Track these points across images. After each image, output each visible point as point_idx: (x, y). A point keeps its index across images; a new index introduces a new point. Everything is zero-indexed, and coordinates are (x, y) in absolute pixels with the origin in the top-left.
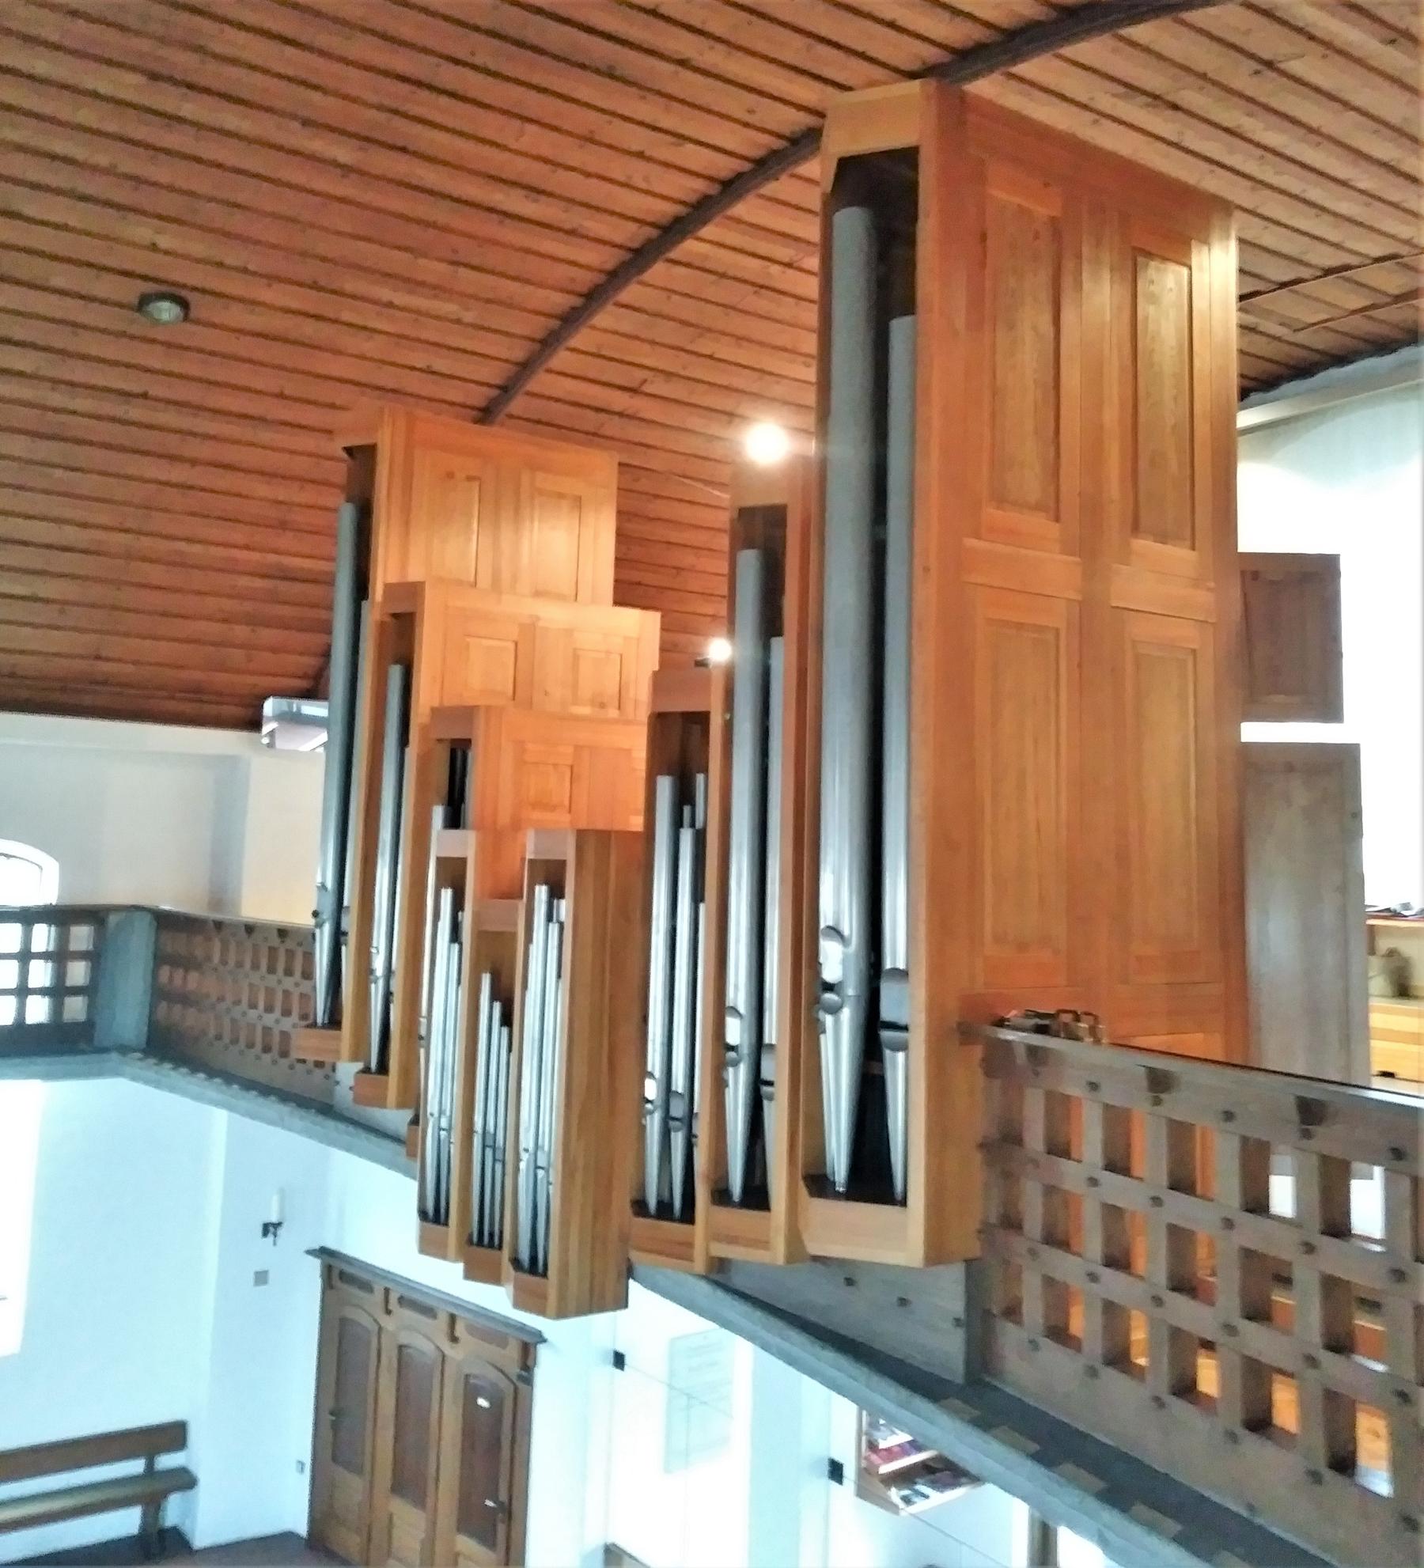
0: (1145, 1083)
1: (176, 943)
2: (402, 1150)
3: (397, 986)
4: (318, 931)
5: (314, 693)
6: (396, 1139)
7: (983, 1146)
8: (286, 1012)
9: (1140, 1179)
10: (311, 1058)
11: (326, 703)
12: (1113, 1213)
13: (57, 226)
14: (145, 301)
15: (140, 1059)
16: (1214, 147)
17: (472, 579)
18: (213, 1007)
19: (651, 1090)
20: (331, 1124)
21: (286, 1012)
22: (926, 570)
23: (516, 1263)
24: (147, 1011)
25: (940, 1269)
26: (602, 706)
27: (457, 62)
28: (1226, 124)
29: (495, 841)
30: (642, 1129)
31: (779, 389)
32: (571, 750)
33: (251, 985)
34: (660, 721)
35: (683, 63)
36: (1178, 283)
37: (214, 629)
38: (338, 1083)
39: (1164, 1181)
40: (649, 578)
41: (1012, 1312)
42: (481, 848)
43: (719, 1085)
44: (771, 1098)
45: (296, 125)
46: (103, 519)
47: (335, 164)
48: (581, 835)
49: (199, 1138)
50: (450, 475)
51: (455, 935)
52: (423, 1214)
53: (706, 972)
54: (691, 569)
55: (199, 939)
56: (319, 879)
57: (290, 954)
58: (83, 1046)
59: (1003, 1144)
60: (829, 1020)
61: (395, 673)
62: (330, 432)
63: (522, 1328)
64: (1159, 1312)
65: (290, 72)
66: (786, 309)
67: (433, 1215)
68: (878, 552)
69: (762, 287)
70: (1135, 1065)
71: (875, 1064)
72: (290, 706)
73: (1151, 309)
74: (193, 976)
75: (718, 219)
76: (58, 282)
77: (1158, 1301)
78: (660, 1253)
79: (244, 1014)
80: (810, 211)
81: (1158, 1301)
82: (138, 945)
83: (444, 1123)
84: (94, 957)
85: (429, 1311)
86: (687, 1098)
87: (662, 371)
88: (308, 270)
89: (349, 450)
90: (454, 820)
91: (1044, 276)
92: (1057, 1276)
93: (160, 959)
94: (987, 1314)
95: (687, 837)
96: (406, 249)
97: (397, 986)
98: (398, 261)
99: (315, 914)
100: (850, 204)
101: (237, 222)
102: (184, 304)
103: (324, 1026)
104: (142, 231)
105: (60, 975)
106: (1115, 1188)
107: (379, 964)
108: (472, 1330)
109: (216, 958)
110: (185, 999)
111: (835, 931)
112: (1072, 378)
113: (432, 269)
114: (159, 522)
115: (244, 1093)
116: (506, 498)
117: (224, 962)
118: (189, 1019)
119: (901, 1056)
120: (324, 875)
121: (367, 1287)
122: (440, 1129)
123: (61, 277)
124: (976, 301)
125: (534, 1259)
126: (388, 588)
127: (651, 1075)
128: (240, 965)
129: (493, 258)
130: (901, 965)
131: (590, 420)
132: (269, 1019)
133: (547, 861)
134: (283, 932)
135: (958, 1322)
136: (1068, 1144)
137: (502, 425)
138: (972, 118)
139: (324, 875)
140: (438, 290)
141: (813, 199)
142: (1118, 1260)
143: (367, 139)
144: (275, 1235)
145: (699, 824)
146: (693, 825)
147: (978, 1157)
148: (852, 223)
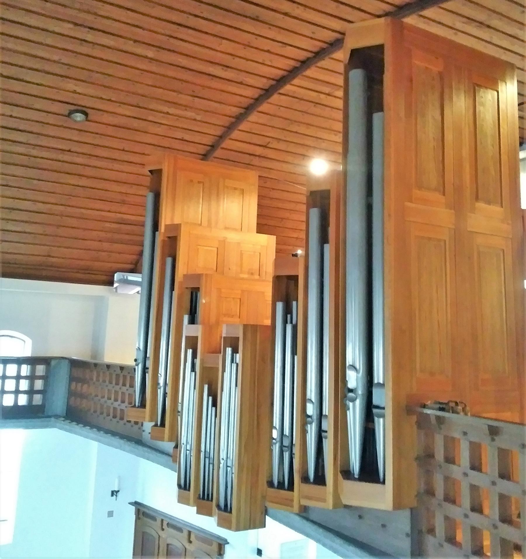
0: (487, 432)
1: (78, 373)
2: (170, 459)
3: (169, 390)
4: (136, 367)
5: (133, 271)
6: (168, 454)
7: (418, 458)
8: (123, 402)
9: (486, 473)
10: (133, 420)
11: (140, 275)
12: (474, 488)
13: (38, 84)
14: (69, 115)
15: (64, 421)
16: (505, 43)
17: (200, 222)
18: (93, 399)
19: (275, 434)
20: (140, 448)
21: (123, 402)
22: (389, 215)
23: (218, 506)
24: (66, 401)
25: (400, 512)
26: (252, 274)
27: (196, 16)
28: (510, 33)
29: (210, 329)
30: (271, 451)
31: (324, 145)
32: (240, 292)
33: (108, 390)
34: (277, 279)
35: (286, 14)
36: (493, 97)
37: (95, 245)
38: (144, 431)
39: (497, 474)
40: (271, 223)
41: (431, 531)
42: (204, 333)
43: (304, 432)
44: (326, 438)
45: (132, 42)
46: (53, 201)
47: (146, 57)
48: (245, 327)
49: (83, 458)
50: (192, 181)
51: (193, 369)
52: (179, 486)
53: (298, 385)
54: (287, 219)
55: (88, 371)
56: (137, 346)
57: (125, 377)
58: (40, 415)
59: (426, 458)
60: (351, 404)
61: (169, 260)
62: (144, 165)
63: (219, 537)
64: (495, 531)
65: (129, 21)
66: (327, 112)
67: (184, 486)
68: (369, 208)
69: (317, 103)
70: (483, 424)
71: (370, 424)
72: (124, 276)
73: (482, 108)
74: (85, 386)
75: (300, 76)
76: (38, 106)
77: (495, 527)
78: (281, 504)
79: (106, 402)
80: (339, 73)
81: (495, 527)
82: (63, 374)
83: (188, 448)
84: (45, 378)
85: (180, 530)
86: (290, 437)
87: (276, 139)
88: (134, 100)
89: (151, 171)
90: (192, 321)
91: (437, 95)
92: (451, 516)
93: (72, 379)
94: (420, 532)
95: (289, 328)
96: (174, 91)
97: (169, 390)
98: (172, 96)
99: (136, 360)
100: (355, 68)
101: (107, 81)
102: (86, 114)
103: (138, 407)
104: (71, 85)
105: (32, 385)
106: (475, 477)
107: (161, 381)
108: (198, 538)
109: (95, 379)
110: (82, 396)
111: (353, 367)
112: (449, 136)
113: (185, 99)
114: (74, 202)
115: (105, 435)
116: (213, 190)
117: (98, 380)
118: (84, 404)
119: (381, 420)
120: (139, 345)
121: (154, 519)
122: (187, 450)
123: (39, 104)
124: (409, 107)
125: (226, 505)
126: (166, 226)
127: (275, 428)
128: (104, 381)
129: (206, 93)
130: (381, 381)
131: (247, 159)
132: (116, 404)
133: (231, 337)
134: (122, 368)
135: (407, 535)
136: (454, 458)
137: (212, 161)
138: (405, 32)
139: (139, 345)
140: (186, 107)
141: (341, 68)
142: (477, 508)
143: (160, 47)
144: (116, 496)
145: (294, 322)
146: (291, 322)
147: (415, 464)
148: (357, 76)
